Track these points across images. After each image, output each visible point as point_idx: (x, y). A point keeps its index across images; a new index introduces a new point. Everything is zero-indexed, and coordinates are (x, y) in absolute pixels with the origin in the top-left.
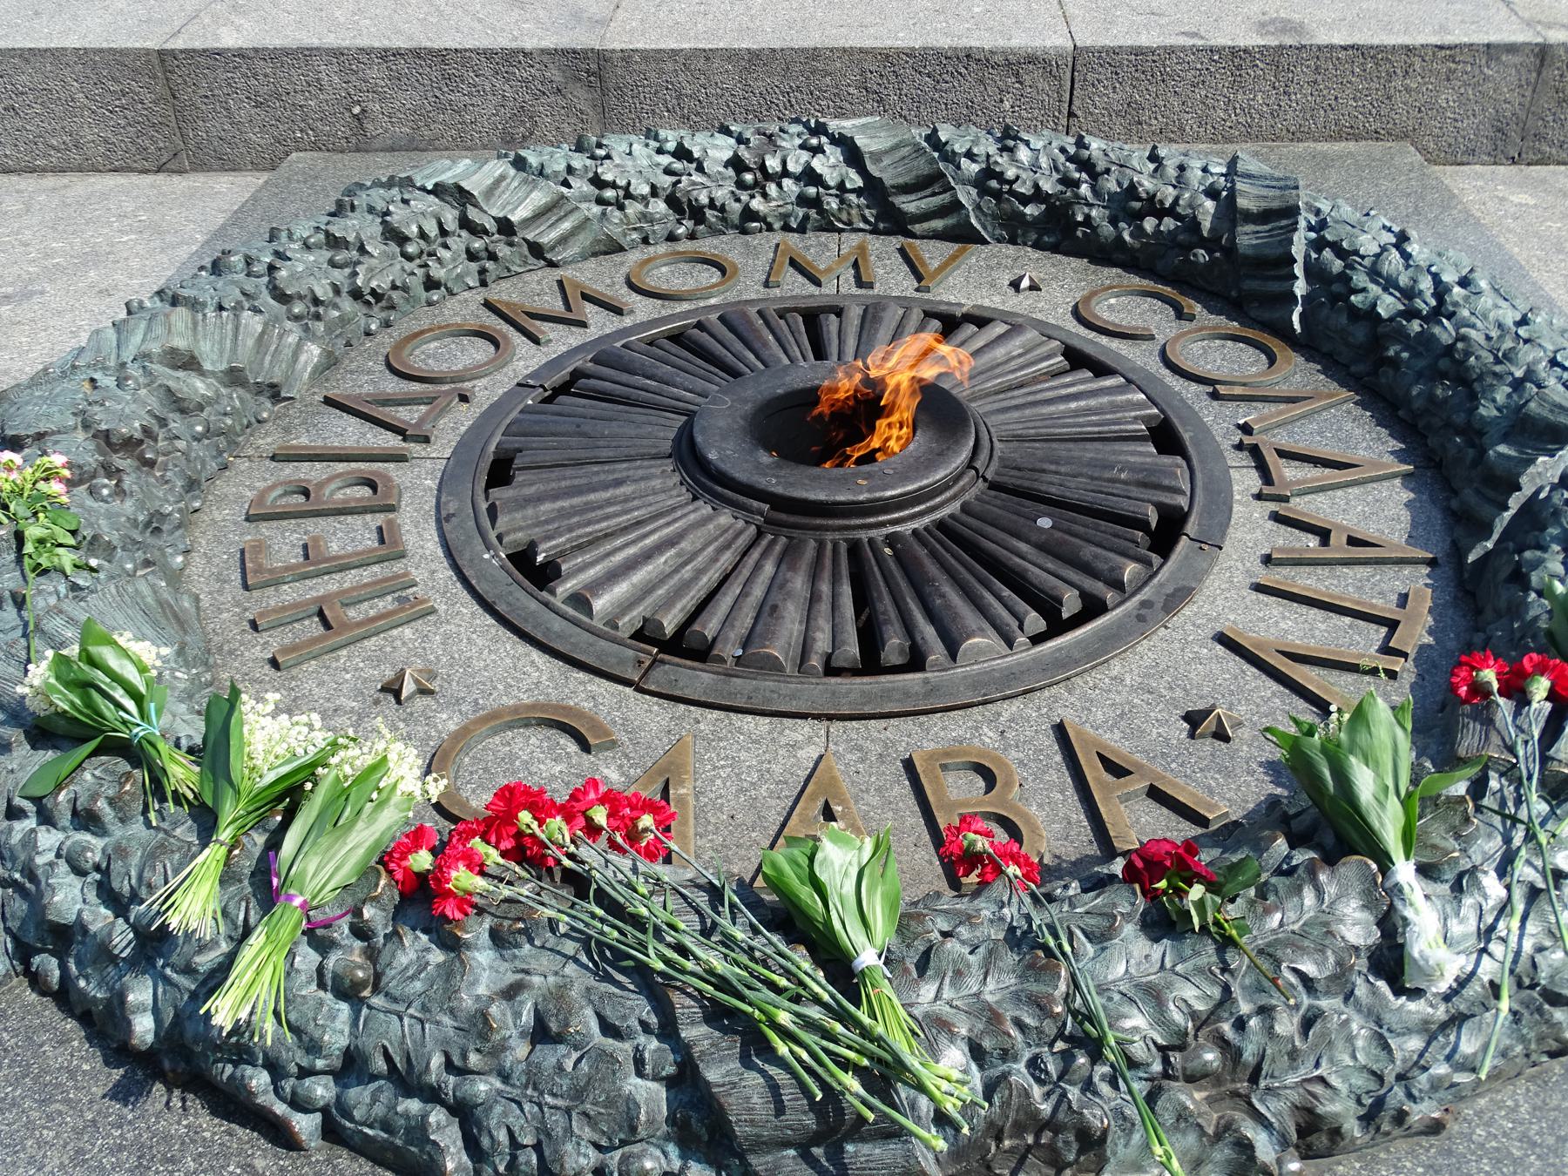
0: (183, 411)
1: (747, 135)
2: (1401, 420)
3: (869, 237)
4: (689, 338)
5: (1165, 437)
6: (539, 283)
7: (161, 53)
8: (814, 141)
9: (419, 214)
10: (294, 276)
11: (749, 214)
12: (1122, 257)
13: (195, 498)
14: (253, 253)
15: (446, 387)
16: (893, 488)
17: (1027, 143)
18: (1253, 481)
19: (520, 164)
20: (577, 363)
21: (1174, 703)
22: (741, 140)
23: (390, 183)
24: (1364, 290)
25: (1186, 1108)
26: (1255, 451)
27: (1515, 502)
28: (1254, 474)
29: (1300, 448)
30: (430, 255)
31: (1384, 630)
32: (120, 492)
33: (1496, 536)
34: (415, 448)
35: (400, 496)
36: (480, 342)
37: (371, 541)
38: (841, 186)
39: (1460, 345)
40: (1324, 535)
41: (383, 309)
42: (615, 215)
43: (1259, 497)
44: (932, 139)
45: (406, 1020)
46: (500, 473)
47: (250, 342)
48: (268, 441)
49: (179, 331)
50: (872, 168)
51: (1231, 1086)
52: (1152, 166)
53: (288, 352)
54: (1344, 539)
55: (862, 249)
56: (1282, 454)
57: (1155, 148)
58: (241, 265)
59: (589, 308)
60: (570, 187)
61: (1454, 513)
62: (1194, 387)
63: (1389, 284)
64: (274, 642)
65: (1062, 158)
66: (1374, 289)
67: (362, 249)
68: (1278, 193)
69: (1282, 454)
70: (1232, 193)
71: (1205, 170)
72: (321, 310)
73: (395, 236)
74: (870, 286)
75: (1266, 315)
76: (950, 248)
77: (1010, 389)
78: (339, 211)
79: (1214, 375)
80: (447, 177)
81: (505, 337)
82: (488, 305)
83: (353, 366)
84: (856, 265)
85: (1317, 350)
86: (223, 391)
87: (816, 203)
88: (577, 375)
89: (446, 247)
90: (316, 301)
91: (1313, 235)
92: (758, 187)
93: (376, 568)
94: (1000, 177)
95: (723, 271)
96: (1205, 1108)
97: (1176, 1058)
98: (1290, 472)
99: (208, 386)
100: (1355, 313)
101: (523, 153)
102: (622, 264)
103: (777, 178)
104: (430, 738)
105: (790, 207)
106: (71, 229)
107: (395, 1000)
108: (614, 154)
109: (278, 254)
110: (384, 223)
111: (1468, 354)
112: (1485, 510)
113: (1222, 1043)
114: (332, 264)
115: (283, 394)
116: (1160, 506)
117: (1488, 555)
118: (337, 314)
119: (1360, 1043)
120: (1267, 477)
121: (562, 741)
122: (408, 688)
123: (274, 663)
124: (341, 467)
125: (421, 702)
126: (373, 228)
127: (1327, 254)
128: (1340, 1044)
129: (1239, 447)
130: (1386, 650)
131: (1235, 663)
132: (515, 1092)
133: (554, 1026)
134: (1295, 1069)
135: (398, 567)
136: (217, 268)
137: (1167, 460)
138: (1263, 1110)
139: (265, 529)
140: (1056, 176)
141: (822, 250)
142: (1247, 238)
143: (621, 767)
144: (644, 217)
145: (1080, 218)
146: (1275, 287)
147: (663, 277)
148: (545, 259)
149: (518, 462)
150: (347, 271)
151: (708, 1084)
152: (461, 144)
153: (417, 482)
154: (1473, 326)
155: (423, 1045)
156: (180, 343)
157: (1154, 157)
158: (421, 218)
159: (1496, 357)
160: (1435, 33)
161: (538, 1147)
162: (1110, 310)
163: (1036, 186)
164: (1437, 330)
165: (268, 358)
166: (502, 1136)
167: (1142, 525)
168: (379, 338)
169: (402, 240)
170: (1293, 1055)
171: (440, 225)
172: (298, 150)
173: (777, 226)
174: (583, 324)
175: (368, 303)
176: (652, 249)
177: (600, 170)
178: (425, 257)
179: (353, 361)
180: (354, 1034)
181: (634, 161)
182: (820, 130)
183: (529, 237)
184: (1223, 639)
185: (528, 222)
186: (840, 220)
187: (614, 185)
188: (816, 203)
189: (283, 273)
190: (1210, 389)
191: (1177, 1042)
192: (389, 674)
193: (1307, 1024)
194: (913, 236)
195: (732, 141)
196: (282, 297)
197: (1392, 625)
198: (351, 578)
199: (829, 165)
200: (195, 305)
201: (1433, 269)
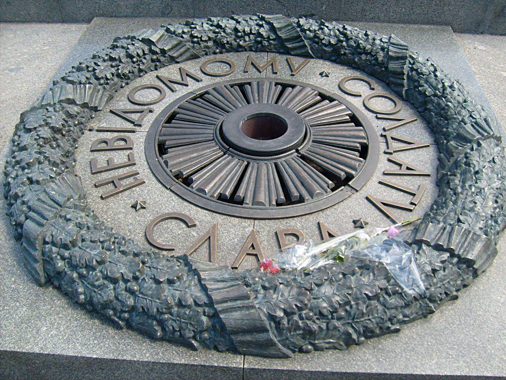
0: (72, 118)
1: (239, 20)
3: (277, 54)
8: (261, 23)
9: (137, 48)
10: (101, 71)
11: (239, 46)
12: (355, 66)
17: (327, 27)
18: (383, 147)
21: (351, 217)
23: (128, 38)
24: (423, 86)
25: (336, 326)
31: (412, 197)
34: (137, 128)
35: (133, 144)
38: (268, 38)
39: (446, 108)
40: (400, 165)
41: (126, 79)
43: (385, 153)
45: (148, 300)
49: (70, 92)
50: (279, 33)
51: (348, 321)
54: (406, 168)
56: (392, 138)
57: (366, 32)
58: (85, 68)
59: (188, 79)
62: (371, 114)
63: (431, 85)
64: (101, 191)
65: (338, 33)
67: (121, 62)
69: (392, 138)
73: (130, 56)
74: (276, 73)
75: (396, 89)
78: (114, 47)
81: (164, 91)
85: (409, 102)
87: (261, 42)
89: (145, 58)
90: (107, 79)
91: (410, 66)
94: (318, 37)
96: (341, 326)
97: (335, 315)
98: (395, 145)
100: (420, 92)
102: (199, 62)
105: (252, 44)
107: (145, 295)
110: (127, 52)
111: (448, 110)
113: (346, 311)
114: (112, 66)
115: (98, 109)
119: (379, 311)
121: (181, 224)
123: (102, 198)
124: (116, 134)
125: (142, 211)
127: (414, 73)
129: (382, 136)
130: (412, 204)
132: (174, 318)
133: (184, 303)
134: (363, 317)
135: (134, 168)
138: (355, 326)
141: (262, 59)
142: (393, 66)
143: (197, 232)
145: (342, 53)
146: (399, 81)
147: (212, 68)
148: (175, 61)
150: (116, 68)
151: (221, 318)
153: (139, 139)
154: (451, 102)
155: (152, 306)
156: (71, 97)
157: (366, 35)
161: (180, 331)
162: (351, 86)
163: (330, 42)
164: (441, 101)
165: (94, 99)
166: (171, 328)
169: (131, 57)
172: (97, 16)
175: (122, 78)
176: (208, 57)
178: (139, 62)
180: (135, 303)
184: (367, 198)
185: (170, 50)
186: (268, 49)
187: (197, 37)
190: (375, 115)
191: (334, 310)
196: (97, 79)
199: (264, 31)
201: (443, 81)
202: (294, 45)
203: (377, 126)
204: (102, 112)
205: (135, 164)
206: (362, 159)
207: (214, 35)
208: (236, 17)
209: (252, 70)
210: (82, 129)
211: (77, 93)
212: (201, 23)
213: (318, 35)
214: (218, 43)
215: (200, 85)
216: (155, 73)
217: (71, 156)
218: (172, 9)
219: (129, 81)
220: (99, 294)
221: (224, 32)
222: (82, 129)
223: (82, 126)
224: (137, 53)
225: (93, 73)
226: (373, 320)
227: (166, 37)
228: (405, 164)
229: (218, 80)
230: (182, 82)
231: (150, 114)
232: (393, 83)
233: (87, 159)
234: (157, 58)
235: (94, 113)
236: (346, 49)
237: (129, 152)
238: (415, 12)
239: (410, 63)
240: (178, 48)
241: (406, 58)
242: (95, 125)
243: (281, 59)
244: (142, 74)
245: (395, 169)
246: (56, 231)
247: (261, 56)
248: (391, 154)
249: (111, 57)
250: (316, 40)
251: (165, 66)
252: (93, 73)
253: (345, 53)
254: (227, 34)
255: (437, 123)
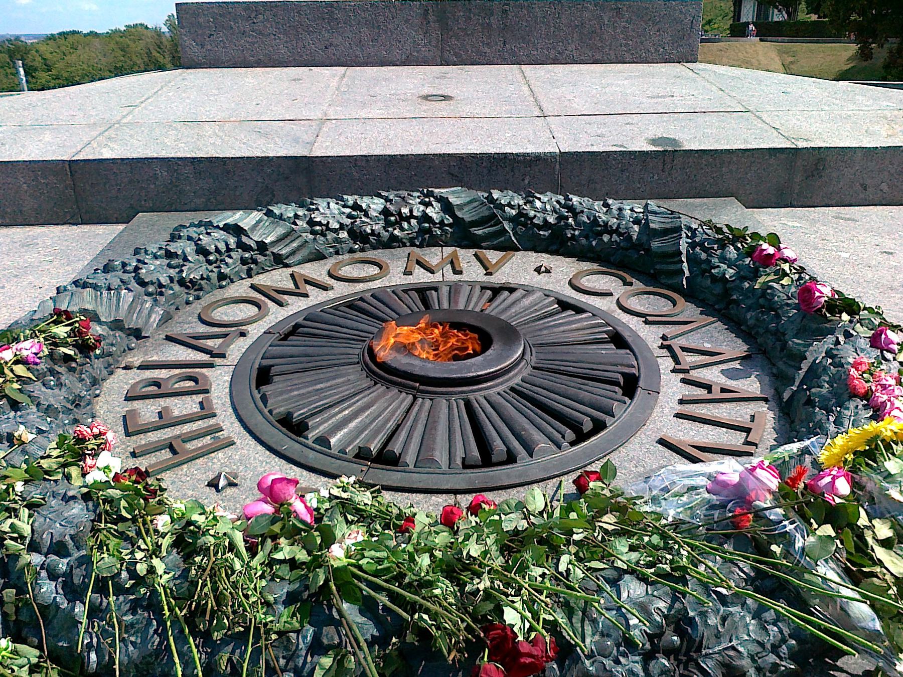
1: (391, 197)
2: (743, 331)
4: (356, 306)
5: (618, 340)
6: (280, 275)
7: (70, 161)
9: (215, 240)
13: (96, 389)
14: (126, 261)
15: (233, 329)
16: (482, 370)
17: (539, 199)
18: (669, 363)
19: (269, 214)
20: (300, 320)
22: (387, 200)
23: (199, 225)
24: (718, 267)
26: (669, 348)
27: (805, 366)
28: (670, 360)
29: (693, 346)
30: (221, 261)
32: (60, 385)
33: (797, 383)
34: (218, 361)
36: (250, 306)
37: (196, 408)
39: (769, 291)
40: (708, 388)
41: (196, 290)
42: (321, 239)
43: (673, 371)
44: (490, 199)
46: (264, 377)
47: (126, 307)
48: (136, 359)
49: (87, 300)
50: (459, 214)
52: (605, 210)
53: (146, 312)
55: (455, 254)
56: (684, 349)
58: (120, 267)
59: (308, 287)
60: (297, 225)
61: (774, 375)
65: (558, 206)
66: (724, 266)
67: (185, 259)
68: (670, 220)
69: (684, 349)
70: (647, 220)
71: (632, 210)
72: (163, 290)
73: (202, 251)
76: (500, 254)
77: (545, 317)
78: (174, 238)
79: (647, 311)
80: (230, 221)
81: (266, 304)
82: (253, 287)
83: (181, 320)
84: (452, 263)
86: (111, 333)
87: (429, 231)
88: (297, 326)
89: (230, 257)
90: (161, 286)
91: (690, 241)
92: (398, 223)
93: (200, 422)
94: (526, 216)
95: (381, 267)
98: (689, 359)
99: (103, 330)
100: (714, 279)
101: (270, 208)
103: (408, 219)
104: (237, 508)
106: (17, 255)
108: (320, 208)
109: (139, 261)
110: (196, 244)
111: (773, 295)
112: (790, 371)
114: (170, 266)
116: (623, 374)
117: (794, 394)
118: (171, 292)
120: (676, 360)
122: (222, 483)
124: (177, 371)
125: (230, 491)
126: (190, 249)
127: (698, 249)
128: (741, 629)
130: (747, 443)
131: (668, 453)
134: (720, 644)
135: (212, 421)
136: (107, 269)
137: (623, 351)
139: (137, 404)
140: (556, 216)
141: (434, 256)
144: (337, 240)
145: (569, 235)
146: (672, 267)
147: (347, 271)
148: (283, 263)
149: (273, 370)
150: (177, 270)
152: (234, 207)
153: (219, 380)
156: (89, 307)
157: (606, 205)
158: (217, 242)
159: (788, 296)
160: (742, 143)
162: (588, 282)
163: (545, 220)
165: (135, 315)
167: (615, 383)
168: (194, 305)
170: (718, 636)
171: (227, 245)
173: (408, 244)
174: (306, 296)
177: (313, 216)
179: (178, 317)
181: (330, 211)
182: (430, 194)
183: (275, 251)
184: (662, 442)
185: (274, 243)
187: (320, 224)
188: (429, 231)
189: (144, 271)
192: (211, 477)
193: (724, 619)
194: (482, 248)
195: (383, 201)
196: (142, 283)
197: (748, 431)
198: (187, 428)
199: (434, 212)
200: (95, 287)
202: (486, 230)
203: (650, 336)
204: (150, 340)
205: (214, 415)
206: (626, 399)
207: (350, 221)
208: (384, 194)
209: (419, 272)
210: (110, 365)
211: (101, 303)
212: (325, 204)
213: (525, 212)
214: (357, 235)
215: (331, 295)
216: (248, 282)
217: (85, 407)
218: (274, 196)
219: (201, 293)
220: (132, 642)
221: (366, 215)
222: (110, 365)
223: (110, 359)
224: (216, 247)
225: (133, 274)
226: (741, 649)
227: (267, 224)
228: (716, 383)
229: (360, 287)
230: (297, 291)
231: (242, 339)
232: (661, 272)
233: (119, 413)
234: (252, 258)
235: (135, 340)
236: (574, 230)
237: (200, 398)
238: (676, 178)
239: (688, 237)
240: (287, 241)
241: (679, 229)
242: (136, 359)
243: (466, 256)
244: (224, 283)
245: (701, 393)
246: (42, 519)
247: (432, 253)
248: (686, 371)
249: (167, 251)
250: (522, 219)
251: (265, 271)
252: (133, 274)
253: (573, 235)
254: (371, 218)
255: (757, 319)
